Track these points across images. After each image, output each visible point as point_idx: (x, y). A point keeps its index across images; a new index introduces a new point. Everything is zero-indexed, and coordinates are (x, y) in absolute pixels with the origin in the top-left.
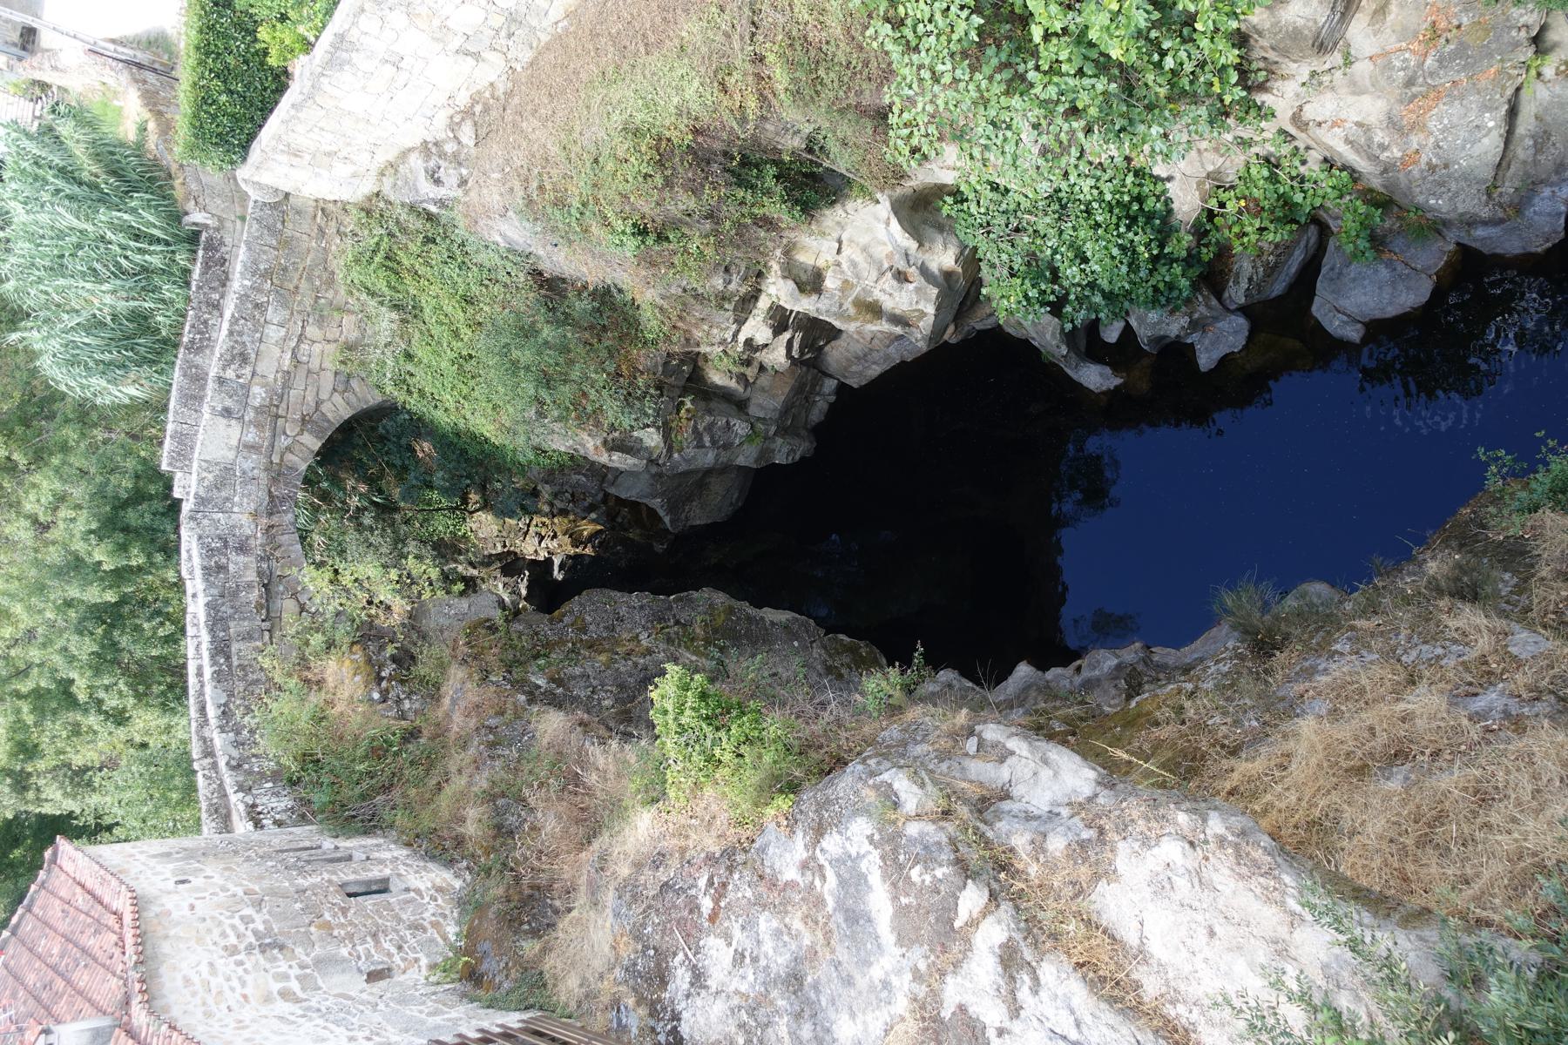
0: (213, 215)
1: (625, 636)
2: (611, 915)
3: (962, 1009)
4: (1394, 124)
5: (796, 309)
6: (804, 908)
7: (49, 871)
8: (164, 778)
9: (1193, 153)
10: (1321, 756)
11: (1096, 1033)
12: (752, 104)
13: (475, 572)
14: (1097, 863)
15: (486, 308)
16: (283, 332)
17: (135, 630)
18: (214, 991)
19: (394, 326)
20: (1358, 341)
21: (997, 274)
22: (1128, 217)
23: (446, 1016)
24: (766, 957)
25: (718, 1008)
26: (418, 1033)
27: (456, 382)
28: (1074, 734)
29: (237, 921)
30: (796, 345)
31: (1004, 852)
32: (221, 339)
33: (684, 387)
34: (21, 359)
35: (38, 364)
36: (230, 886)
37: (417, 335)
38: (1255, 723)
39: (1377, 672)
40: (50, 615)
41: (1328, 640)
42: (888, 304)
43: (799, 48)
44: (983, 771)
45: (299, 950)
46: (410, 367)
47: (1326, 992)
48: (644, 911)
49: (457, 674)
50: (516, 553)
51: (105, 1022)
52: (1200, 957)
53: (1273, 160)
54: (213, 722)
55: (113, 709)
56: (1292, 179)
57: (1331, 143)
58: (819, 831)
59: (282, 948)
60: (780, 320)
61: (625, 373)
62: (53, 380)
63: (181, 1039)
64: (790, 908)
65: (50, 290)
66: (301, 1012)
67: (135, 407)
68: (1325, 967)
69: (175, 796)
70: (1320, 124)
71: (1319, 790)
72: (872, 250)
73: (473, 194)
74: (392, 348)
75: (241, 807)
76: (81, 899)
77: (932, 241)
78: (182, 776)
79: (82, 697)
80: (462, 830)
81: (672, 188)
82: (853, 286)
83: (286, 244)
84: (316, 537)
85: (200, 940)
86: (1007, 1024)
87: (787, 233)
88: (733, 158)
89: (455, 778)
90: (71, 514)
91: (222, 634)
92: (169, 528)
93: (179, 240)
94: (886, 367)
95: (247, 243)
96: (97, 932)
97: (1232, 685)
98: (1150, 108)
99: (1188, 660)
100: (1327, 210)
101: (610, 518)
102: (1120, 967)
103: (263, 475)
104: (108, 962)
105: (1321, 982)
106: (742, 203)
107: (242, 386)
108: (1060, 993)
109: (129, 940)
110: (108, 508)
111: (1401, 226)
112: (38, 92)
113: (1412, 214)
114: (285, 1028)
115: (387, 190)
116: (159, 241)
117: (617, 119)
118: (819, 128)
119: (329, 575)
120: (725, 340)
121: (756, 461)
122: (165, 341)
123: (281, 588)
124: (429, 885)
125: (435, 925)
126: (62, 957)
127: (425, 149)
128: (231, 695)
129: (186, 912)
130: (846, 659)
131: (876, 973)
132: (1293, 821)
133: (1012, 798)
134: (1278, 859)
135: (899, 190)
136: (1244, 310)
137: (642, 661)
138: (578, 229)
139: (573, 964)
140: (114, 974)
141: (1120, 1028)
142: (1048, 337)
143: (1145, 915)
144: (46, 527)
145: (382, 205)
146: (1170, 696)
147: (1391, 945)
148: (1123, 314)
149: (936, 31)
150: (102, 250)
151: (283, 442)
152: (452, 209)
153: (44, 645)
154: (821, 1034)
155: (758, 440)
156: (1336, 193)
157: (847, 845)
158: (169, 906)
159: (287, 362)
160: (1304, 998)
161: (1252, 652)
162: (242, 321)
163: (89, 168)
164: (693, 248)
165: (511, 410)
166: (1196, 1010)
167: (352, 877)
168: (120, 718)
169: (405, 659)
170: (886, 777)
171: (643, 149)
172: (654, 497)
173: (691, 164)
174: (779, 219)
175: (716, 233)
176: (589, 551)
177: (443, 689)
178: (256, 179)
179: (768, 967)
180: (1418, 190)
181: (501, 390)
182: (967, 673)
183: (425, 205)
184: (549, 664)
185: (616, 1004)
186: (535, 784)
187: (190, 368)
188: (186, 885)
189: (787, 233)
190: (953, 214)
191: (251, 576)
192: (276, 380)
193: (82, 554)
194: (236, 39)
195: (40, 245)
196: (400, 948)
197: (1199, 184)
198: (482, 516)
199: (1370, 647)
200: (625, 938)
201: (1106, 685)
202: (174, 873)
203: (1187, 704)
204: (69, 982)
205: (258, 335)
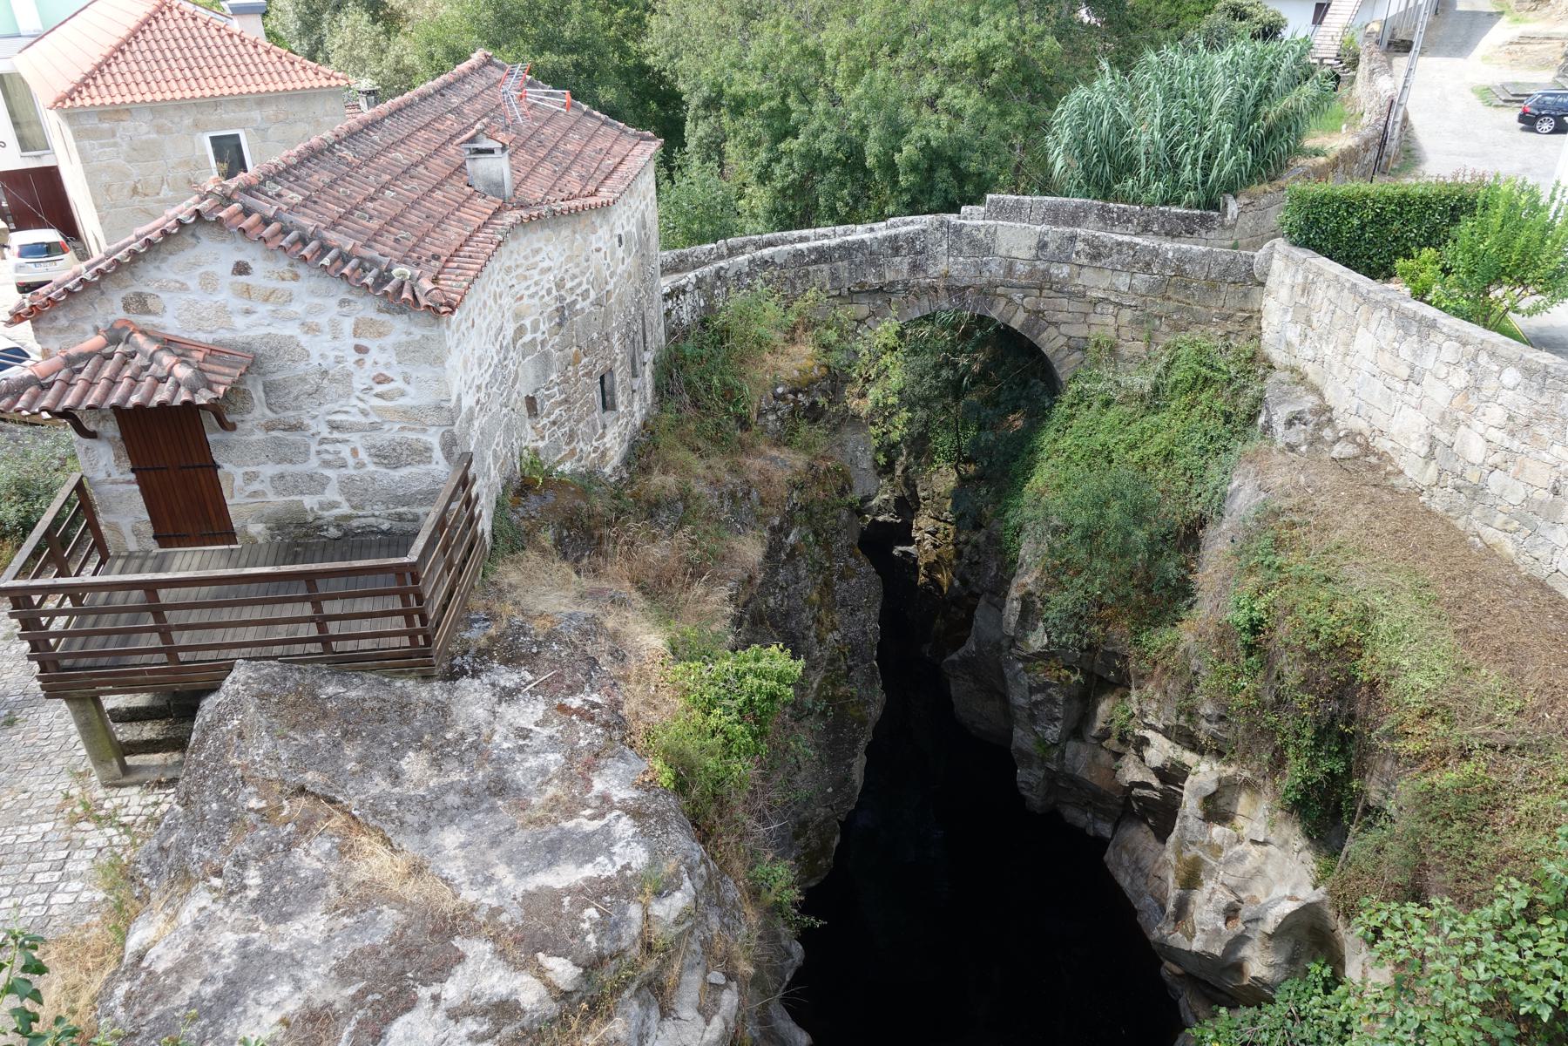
0: (1236, 220)
2: (571, 611)
3: (461, 958)
5: (1185, 793)
6: (566, 798)
7: (634, 135)
12: (1412, 746)
13: (898, 473)
15: (1161, 475)
17: (841, 183)
18: (527, 273)
19: (1137, 389)
21: (1245, 1027)
25: (480, 713)
26: (479, 443)
29: (584, 287)
30: (1146, 792)
31: (608, 1009)
33: (1092, 673)
34: (1084, 71)
36: (615, 279)
37: (1129, 410)
40: (854, 115)
42: (1199, 896)
43: (1484, 799)
44: (690, 989)
45: (557, 339)
46: (1096, 405)
49: (800, 461)
50: (918, 509)
51: (508, 190)
54: (759, 253)
58: (637, 814)
59: (560, 325)
60: (1172, 775)
61: (1104, 613)
62: (1067, 99)
65: (1151, 90)
67: (1046, 169)
72: (1259, 879)
73: (1280, 457)
75: (683, 282)
76: (610, 162)
77: (1276, 950)
79: (782, 146)
81: (1307, 660)
82: (1216, 857)
83: (1212, 286)
84: (928, 329)
86: (443, 1005)
88: (1348, 725)
90: (944, 124)
94: (1129, 893)
95: (1210, 253)
96: (582, 177)
103: (984, 280)
106: (1298, 735)
107: (1069, 257)
109: (573, 204)
112: (1347, 60)
114: (492, 333)
115: (1278, 375)
116: (1206, 175)
119: (891, 343)
120: (1146, 716)
121: (1019, 750)
122: (1109, 188)
123: (879, 302)
124: (608, 445)
125: (573, 452)
126: (563, 153)
127: (1324, 413)
128: (782, 267)
130: (815, 843)
131: (501, 871)
133: (662, 1019)
138: (1251, 563)
139: (529, 577)
145: (1261, 371)
149: (1525, 962)
151: (1017, 296)
152: (1262, 438)
153: (827, 113)
157: (623, 843)
158: (600, 232)
159: (1094, 294)
163: (1272, 111)
164: (1243, 682)
165: (1058, 502)
167: (618, 379)
168: (764, 177)
169: (814, 414)
170: (687, 884)
171: (1346, 629)
172: (976, 644)
173: (1335, 679)
174: (1284, 776)
176: (922, 579)
177: (786, 449)
179: (514, 761)
183: (1264, 412)
184: (809, 546)
185: (492, 617)
186: (695, 537)
188: (617, 244)
189: (1269, 783)
190: (1311, 976)
191: (890, 276)
192: (1076, 285)
193: (908, 136)
194: (1419, 228)
195: (1193, 78)
196: (554, 423)
198: (954, 477)
200: (549, 625)
202: (629, 232)
204: (543, 159)
205: (1119, 267)
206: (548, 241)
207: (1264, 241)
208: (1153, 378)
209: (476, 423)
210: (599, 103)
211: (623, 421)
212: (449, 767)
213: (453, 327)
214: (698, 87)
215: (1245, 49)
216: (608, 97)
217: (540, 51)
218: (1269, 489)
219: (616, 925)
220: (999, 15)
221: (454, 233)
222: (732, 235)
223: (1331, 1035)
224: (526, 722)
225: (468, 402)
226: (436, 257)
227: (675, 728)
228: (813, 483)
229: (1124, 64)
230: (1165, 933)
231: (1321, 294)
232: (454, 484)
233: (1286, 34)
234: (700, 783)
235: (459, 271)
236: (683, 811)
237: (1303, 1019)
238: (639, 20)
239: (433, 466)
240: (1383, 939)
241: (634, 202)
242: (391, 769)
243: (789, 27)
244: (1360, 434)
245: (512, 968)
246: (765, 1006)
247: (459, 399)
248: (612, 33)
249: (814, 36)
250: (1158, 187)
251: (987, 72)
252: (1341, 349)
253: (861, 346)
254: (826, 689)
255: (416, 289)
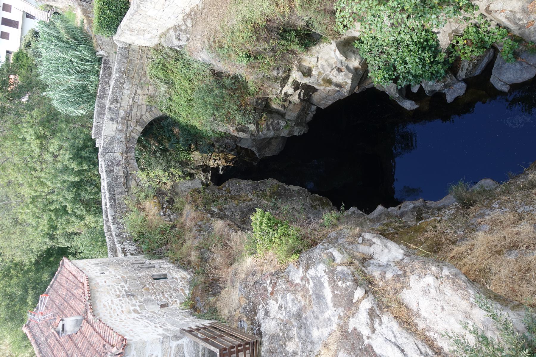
0: (106, 52)
1: (243, 194)
2: (238, 291)
3: (355, 329)
4: (525, 11)
5: (302, 82)
6: (302, 292)
7: (61, 268)
8: (96, 238)
9: (448, 23)
10: (485, 246)
11: (401, 340)
12: (287, 10)
13: (194, 171)
14: (403, 282)
15: (196, 83)
16: (129, 92)
19: (166, 90)
20: (507, 91)
21: (374, 68)
22: (422, 47)
23: (186, 320)
24: (289, 307)
25: (273, 323)
26: (177, 326)
27: (186, 108)
28: (397, 234)
29: (119, 287)
30: (302, 94)
31: (371, 277)
32: (109, 95)
33: (263, 109)
34: (46, 101)
35: (52, 103)
36: (117, 275)
37: (173, 92)
38: (462, 233)
39: (508, 216)
40: (59, 185)
41: (490, 204)
42: (334, 80)
44: (364, 249)
45: (139, 297)
46: (171, 103)
47: (483, 331)
48: (249, 290)
49: (188, 207)
50: (207, 165)
51: (79, 318)
52: (438, 316)
53: (477, 25)
55: (79, 215)
56: (485, 32)
57: (500, 19)
58: (307, 268)
59: (133, 296)
60: (296, 86)
61: (243, 105)
62: (57, 108)
63: (103, 325)
64: (297, 292)
65: (55, 78)
66: (140, 317)
67: (83, 116)
68: (483, 322)
69: (99, 244)
70: (496, 12)
71: (484, 258)
73: (191, 44)
74: (165, 97)
75: (120, 249)
76: (71, 277)
77: (351, 57)
78: (101, 237)
79: (70, 211)
80: (190, 259)
81: (259, 41)
82: (322, 74)
83: (130, 62)
84: (142, 160)
85: (108, 293)
86: (370, 335)
87: (299, 55)
88: (280, 29)
89: (187, 241)
91: (112, 192)
92: (95, 157)
93: (95, 60)
94: (334, 101)
95: (117, 62)
96: (76, 289)
97: (454, 218)
98: (431, 8)
99: (439, 206)
100: (497, 43)
101: (238, 153)
102: (410, 318)
104: (80, 298)
105: (481, 327)
106: (284, 45)
107: (117, 110)
108: (389, 326)
109: (86, 292)
110: (75, 150)
111: (525, 49)
112: (49, 9)
113: (530, 44)
114: (135, 322)
115: (162, 43)
117: (240, 17)
118: (311, 18)
119: (146, 174)
120: (277, 93)
121: (288, 135)
122: (92, 95)
123: (131, 178)
124: (180, 277)
125: (182, 290)
126: (66, 296)
127: (175, 28)
128: (116, 212)
129: (104, 283)
130: (318, 203)
131: (326, 315)
132: (474, 269)
133: (374, 259)
134: (468, 284)
135: (339, 39)
136: (464, 80)
137: (249, 203)
138: (227, 56)
140: (82, 302)
141: (409, 339)
142: (392, 91)
143: (419, 301)
144: (56, 156)
145: (161, 48)
146: (431, 221)
147: (507, 316)
148: (420, 82)
150: (71, 64)
151: (130, 129)
152: (184, 49)
153: (57, 195)
154: (307, 334)
155: (288, 128)
156: (501, 37)
157: (317, 272)
158: (98, 281)
159: (131, 102)
160: (475, 332)
161: (462, 207)
162: (116, 88)
163: (66, 37)
164: (266, 61)
165: (205, 118)
166: (436, 334)
167: (155, 273)
168: (82, 218)
169: (171, 202)
170: (330, 250)
171: (249, 27)
173: (265, 32)
174: (296, 51)
175: (274, 56)
176: (231, 164)
177: (184, 212)
178: (119, 39)
179: (290, 311)
180: (533, 35)
181: (202, 112)
182: (360, 208)
184: (218, 204)
185: (240, 320)
186: (214, 245)
187: (100, 104)
188: (103, 274)
189: (299, 55)
190: (358, 47)
191: (121, 174)
192: (127, 108)
193: (68, 165)
195: (51, 63)
196: (171, 297)
197: (449, 34)
198: (195, 153)
199: (506, 206)
200: (243, 299)
201: (409, 214)
203: (438, 225)
204: (68, 304)
205: (121, 93)
206: (100, 301)
207: (114, 43)
208: (162, 84)
209: (169, 327)
210: (49, 280)
211: (171, 271)
212: (292, 334)
213: (132, 338)
214: (45, 242)
215: (41, 45)
216: (46, 276)
217: (26, 303)
218: (202, 48)
219: (344, 275)
220: (22, 131)
221: (95, 339)
222: (103, 230)
223: (376, 43)
224: (276, 307)
225: (161, 331)
226: (104, 346)
227: (279, 253)
228: (196, 202)
229: (44, 87)
230: (346, 91)
231: (134, 26)
232: (191, 335)
233: (37, 29)
234: (297, 245)
235: (110, 337)
236: (307, 251)
237: (371, 51)
238: (16, 265)
239: (184, 344)
240: (347, 24)
241: (87, 268)
242: (292, 356)
243: (22, 209)
244: (184, 17)
245: (358, 311)
246: (370, 220)
247: (159, 335)
248: (21, 275)
249: (27, 199)
250: (92, 78)
251: (45, 136)
252: (154, 21)
253: (147, 185)
254: (267, 199)
255: (116, 353)
